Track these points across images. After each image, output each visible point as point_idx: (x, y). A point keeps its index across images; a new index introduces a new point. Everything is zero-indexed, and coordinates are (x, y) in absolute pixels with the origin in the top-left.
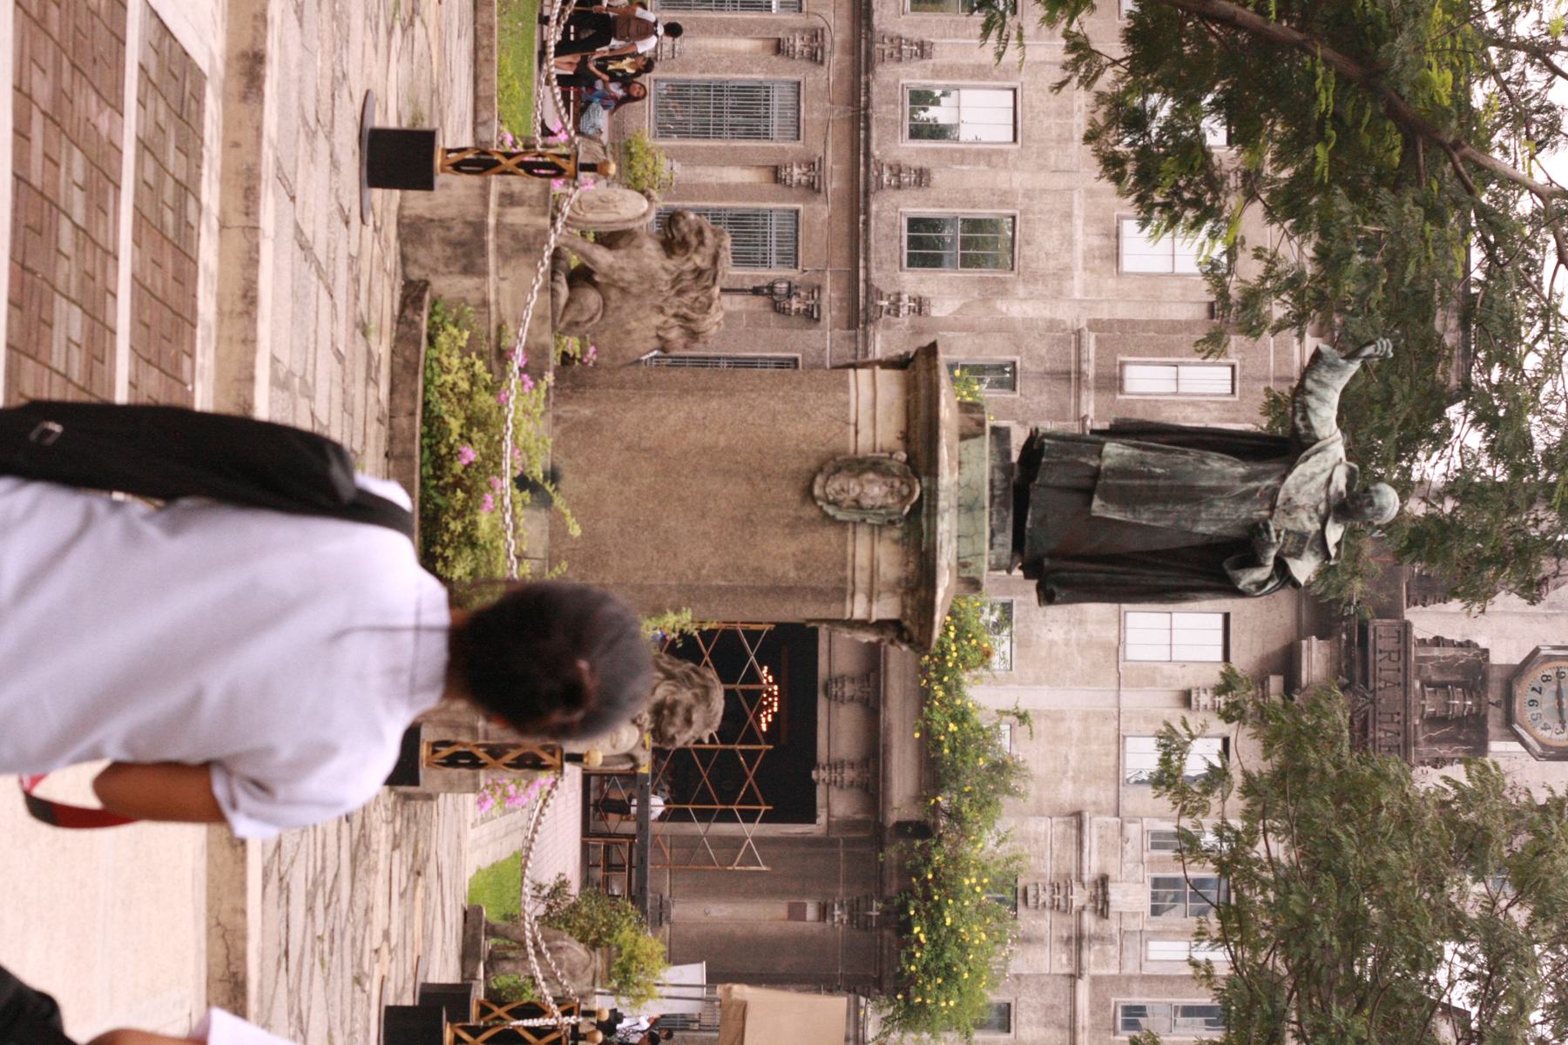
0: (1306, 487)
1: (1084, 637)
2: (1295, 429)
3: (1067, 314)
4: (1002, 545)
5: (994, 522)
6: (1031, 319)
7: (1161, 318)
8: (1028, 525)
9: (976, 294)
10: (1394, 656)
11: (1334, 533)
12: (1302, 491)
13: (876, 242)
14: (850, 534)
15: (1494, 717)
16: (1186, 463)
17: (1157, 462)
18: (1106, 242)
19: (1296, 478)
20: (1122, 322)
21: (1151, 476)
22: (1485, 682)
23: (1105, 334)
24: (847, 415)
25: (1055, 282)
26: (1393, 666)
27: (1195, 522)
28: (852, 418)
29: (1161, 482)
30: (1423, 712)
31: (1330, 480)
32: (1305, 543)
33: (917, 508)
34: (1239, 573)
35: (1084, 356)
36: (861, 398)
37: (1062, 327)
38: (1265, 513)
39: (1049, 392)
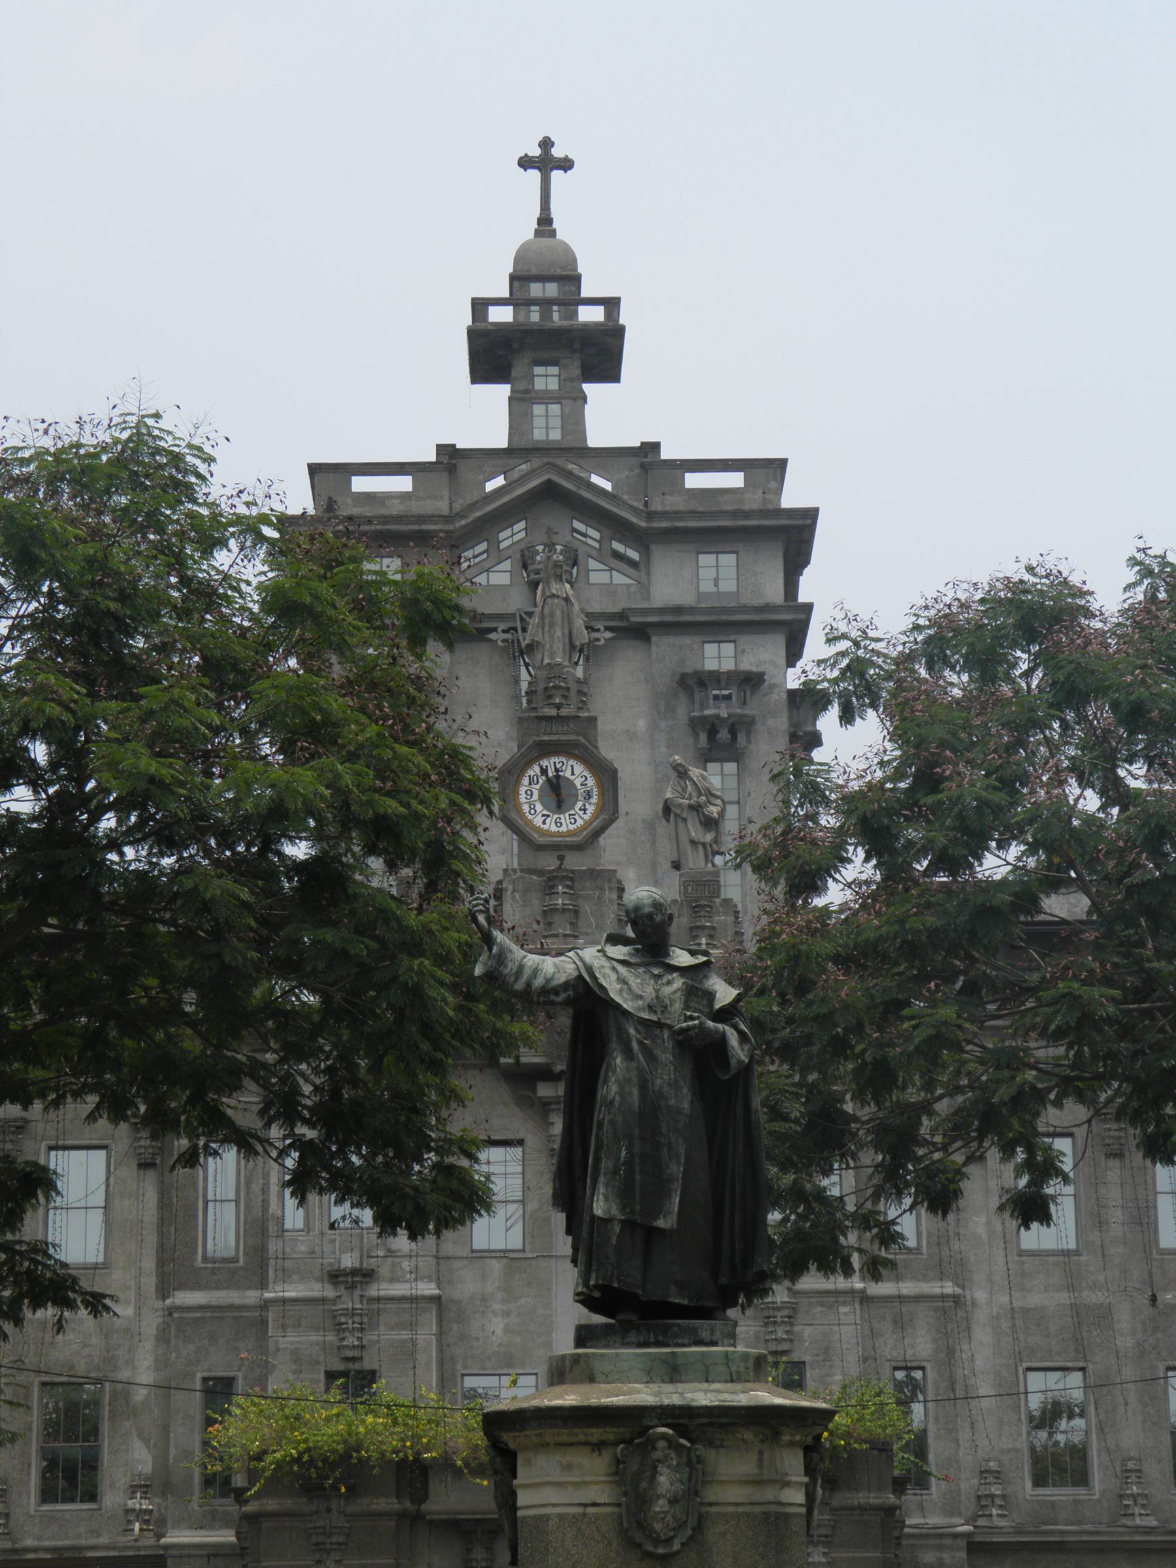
0: (634, 986)
1: (499, 1295)
2: (568, 1003)
3: (151, 1324)
4: (712, 1331)
5: (686, 1341)
6: (156, 1361)
8: (686, 1302)
9: (128, 1424)
12: (639, 992)
13: (68, 1538)
14: (713, 1509)
16: (613, 1123)
19: (625, 1000)
21: (629, 1162)
24: (574, 1516)
28: (580, 1510)
29: (637, 1150)
31: (623, 962)
32: (697, 988)
33: (681, 1430)
34: (733, 1061)
36: (554, 1501)
38: (666, 1034)
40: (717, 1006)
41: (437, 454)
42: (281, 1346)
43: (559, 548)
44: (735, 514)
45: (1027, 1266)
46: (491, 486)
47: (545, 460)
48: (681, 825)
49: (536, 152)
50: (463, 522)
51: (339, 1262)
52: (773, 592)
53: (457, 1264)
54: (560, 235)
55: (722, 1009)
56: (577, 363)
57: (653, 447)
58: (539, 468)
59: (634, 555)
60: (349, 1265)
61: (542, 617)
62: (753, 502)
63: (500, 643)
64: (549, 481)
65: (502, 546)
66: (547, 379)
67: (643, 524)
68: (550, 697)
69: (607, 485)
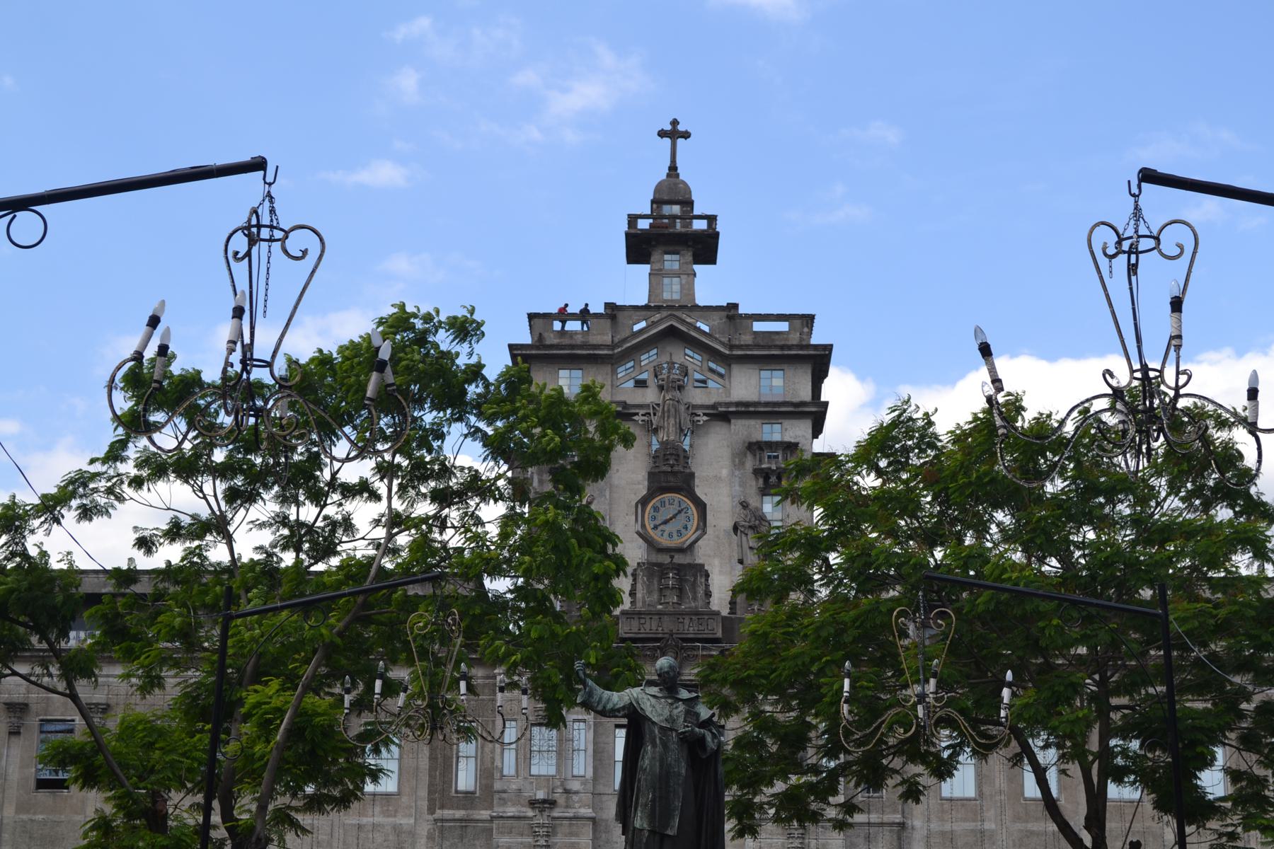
3: (424, 829)
7: (427, 767)
10: (642, 621)
11: (684, 694)
15: (680, 559)
17: (646, 797)
18: (377, 803)
19: (654, 716)
20: (430, 792)
21: (653, 800)
22: (659, 565)
23: (437, 803)
25: (403, 835)
26: (648, 621)
27: (679, 774)
29: (657, 795)
30: (677, 603)
31: (654, 696)
34: (709, 748)
35: (450, 817)
37: (432, 831)
39: (474, 840)
40: (701, 720)
41: (605, 308)
42: (500, 844)
43: (676, 366)
44: (782, 347)
45: (945, 806)
46: (637, 328)
47: (669, 313)
48: (744, 538)
49: (668, 127)
50: (620, 350)
51: (535, 795)
52: (805, 394)
53: (605, 798)
54: (681, 177)
55: (704, 721)
56: (690, 254)
57: (735, 306)
58: (666, 317)
59: (722, 371)
60: (542, 797)
61: (663, 412)
62: (794, 339)
63: (640, 422)
64: (671, 325)
65: (643, 364)
66: (671, 262)
67: (727, 352)
68: (667, 460)
69: (706, 328)
